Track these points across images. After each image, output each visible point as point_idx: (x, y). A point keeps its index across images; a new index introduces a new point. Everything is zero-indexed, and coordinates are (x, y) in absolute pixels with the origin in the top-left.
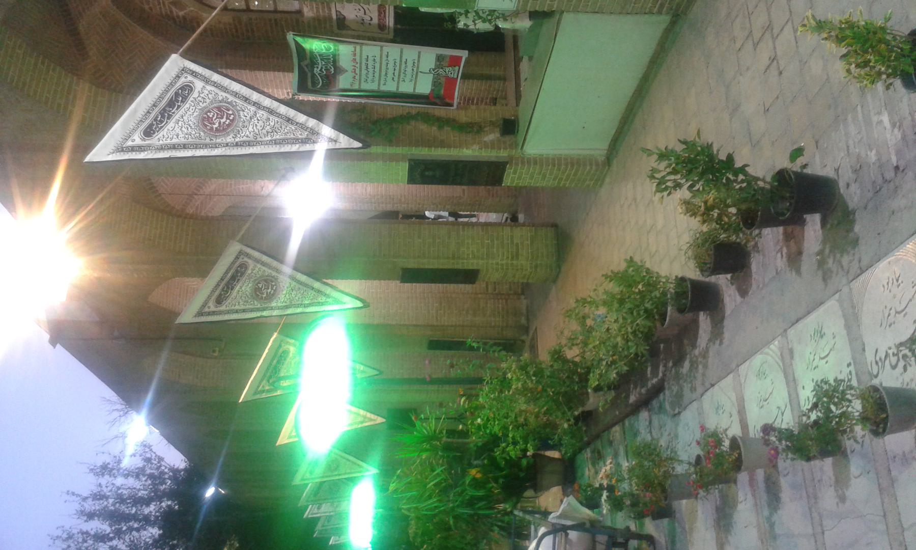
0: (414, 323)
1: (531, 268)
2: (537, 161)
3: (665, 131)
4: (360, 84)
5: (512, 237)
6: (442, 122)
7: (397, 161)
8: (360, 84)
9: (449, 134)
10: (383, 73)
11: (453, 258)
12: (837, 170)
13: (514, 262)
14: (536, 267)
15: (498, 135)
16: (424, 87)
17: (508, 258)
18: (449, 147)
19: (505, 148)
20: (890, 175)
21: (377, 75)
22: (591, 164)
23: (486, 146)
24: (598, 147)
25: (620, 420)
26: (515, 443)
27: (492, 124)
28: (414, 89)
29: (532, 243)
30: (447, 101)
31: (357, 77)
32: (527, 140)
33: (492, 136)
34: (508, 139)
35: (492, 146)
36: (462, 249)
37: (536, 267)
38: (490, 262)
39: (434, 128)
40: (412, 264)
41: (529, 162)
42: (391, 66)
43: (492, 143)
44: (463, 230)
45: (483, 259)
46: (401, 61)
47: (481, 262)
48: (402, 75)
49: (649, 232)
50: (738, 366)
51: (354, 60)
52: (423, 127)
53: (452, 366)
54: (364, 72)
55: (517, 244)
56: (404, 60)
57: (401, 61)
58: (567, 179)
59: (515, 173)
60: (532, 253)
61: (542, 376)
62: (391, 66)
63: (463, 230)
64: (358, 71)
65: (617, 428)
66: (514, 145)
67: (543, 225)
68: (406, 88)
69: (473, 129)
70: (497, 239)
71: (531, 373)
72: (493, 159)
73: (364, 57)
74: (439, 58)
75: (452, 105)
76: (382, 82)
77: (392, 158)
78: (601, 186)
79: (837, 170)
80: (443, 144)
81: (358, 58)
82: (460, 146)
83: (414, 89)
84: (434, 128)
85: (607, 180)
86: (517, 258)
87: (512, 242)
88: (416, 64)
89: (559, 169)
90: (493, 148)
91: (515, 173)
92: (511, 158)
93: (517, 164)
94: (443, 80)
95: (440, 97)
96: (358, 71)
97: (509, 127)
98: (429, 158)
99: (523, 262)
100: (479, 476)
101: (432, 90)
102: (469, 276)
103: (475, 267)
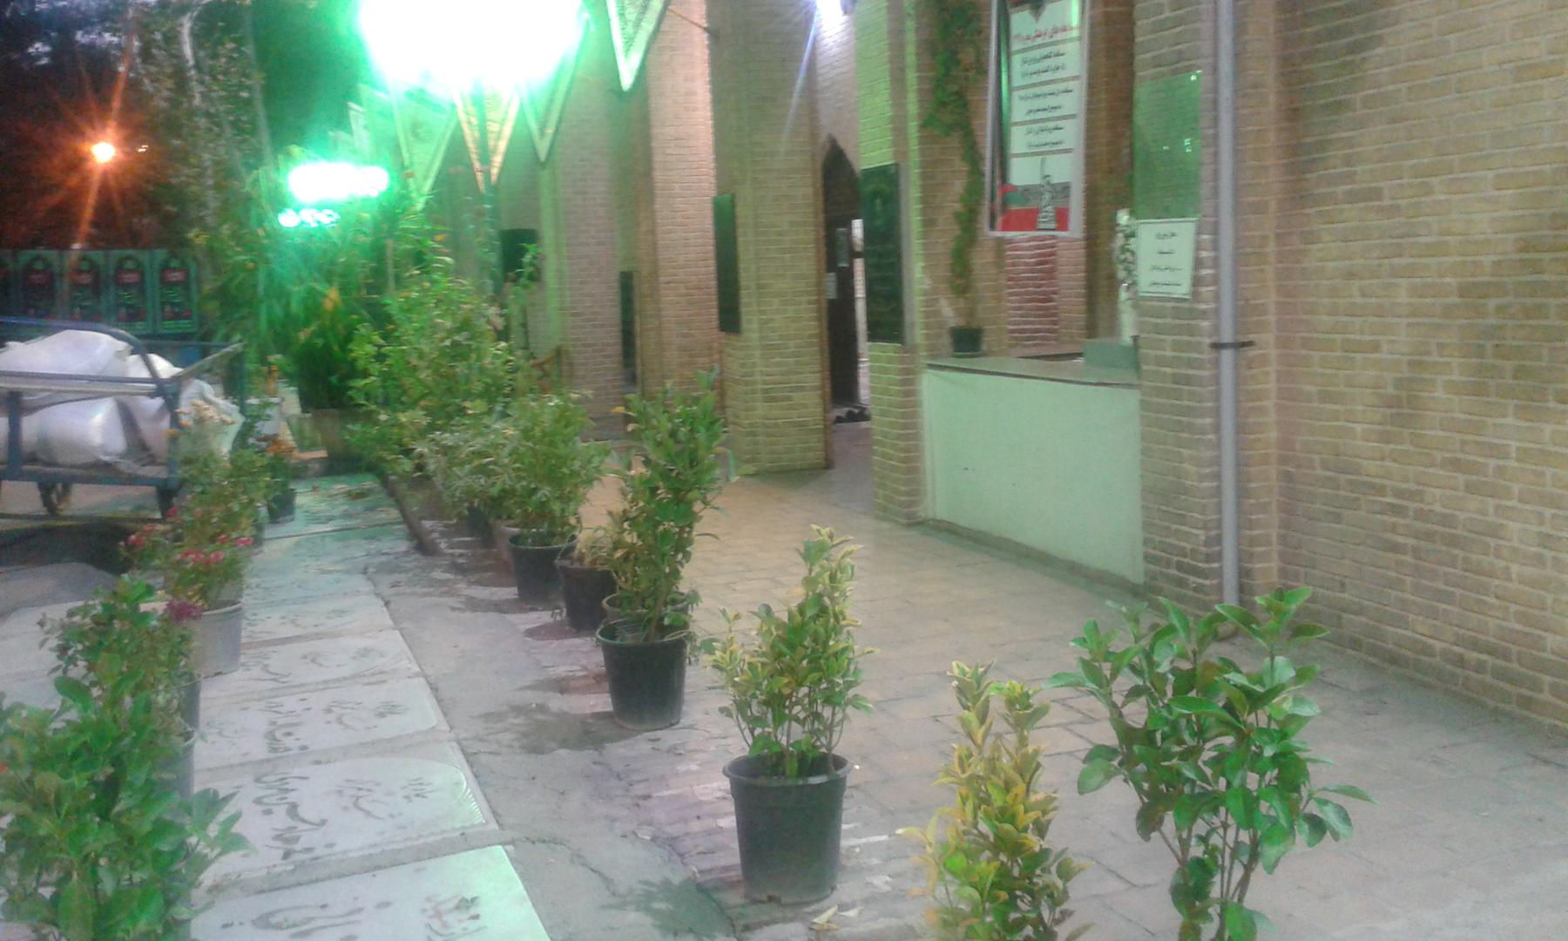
0: (661, 243)
1: (751, 425)
2: (909, 393)
3: (1194, 833)
4: (1019, 52)
5: (801, 389)
6: (968, 221)
7: (895, 144)
8: (1019, 52)
9: (948, 233)
10: (1037, 90)
11: (760, 287)
12: (691, 727)
13: (759, 396)
14: (754, 434)
15: (953, 323)
16: (1022, 173)
17: (766, 383)
18: (925, 235)
19: (928, 337)
20: (639, 789)
21: (1036, 79)
22: (908, 494)
23: (930, 301)
24: (939, 502)
25: (406, 518)
26: (380, 357)
27: (971, 313)
28: (1017, 155)
29: (794, 424)
30: (999, 220)
31: (1029, 43)
32: (945, 373)
33: (949, 313)
34: (946, 340)
35: (932, 313)
36: (776, 300)
37: (754, 434)
38: (757, 353)
39: (958, 206)
40: (743, 213)
41: (910, 382)
42: (1051, 101)
43: (937, 313)
44: (809, 303)
45: (762, 338)
46: (1059, 118)
47: (755, 335)
48: (1036, 126)
49: (773, 580)
50: (401, 630)
51: (1056, 31)
52: (958, 186)
53: (480, 214)
54: (1037, 53)
55: (789, 399)
56: (1060, 123)
57: (1059, 118)
58: (884, 455)
59: (890, 361)
60: (776, 425)
61: (454, 358)
62: (1051, 101)
63: (809, 303)
64: (1039, 41)
65: (394, 514)
66: (934, 352)
67: (828, 446)
68: (1018, 140)
69: (960, 276)
70: (797, 363)
71: (457, 338)
72: (907, 318)
73: (1061, 48)
74: (1065, 189)
75: (992, 227)
76: (1022, 93)
77: (899, 132)
78: (877, 517)
79: (691, 727)
80: (928, 223)
81: (1059, 37)
82: (928, 256)
83: (1017, 155)
84: (958, 206)
85: (885, 525)
86: (768, 400)
87: (793, 390)
88: (1057, 149)
89: (899, 437)
90: (927, 315)
91: (890, 361)
92: (913, 350)
93: (902, 361)
94: (1031, 205)
95: (1017, 211)
96: (1039, 41)
97: (967, 341)
98: (903, 202)
99: (761, 409)
100: (328, 305)
101: (1014, 188)
102: (729, 319)
103: (744, 325)
